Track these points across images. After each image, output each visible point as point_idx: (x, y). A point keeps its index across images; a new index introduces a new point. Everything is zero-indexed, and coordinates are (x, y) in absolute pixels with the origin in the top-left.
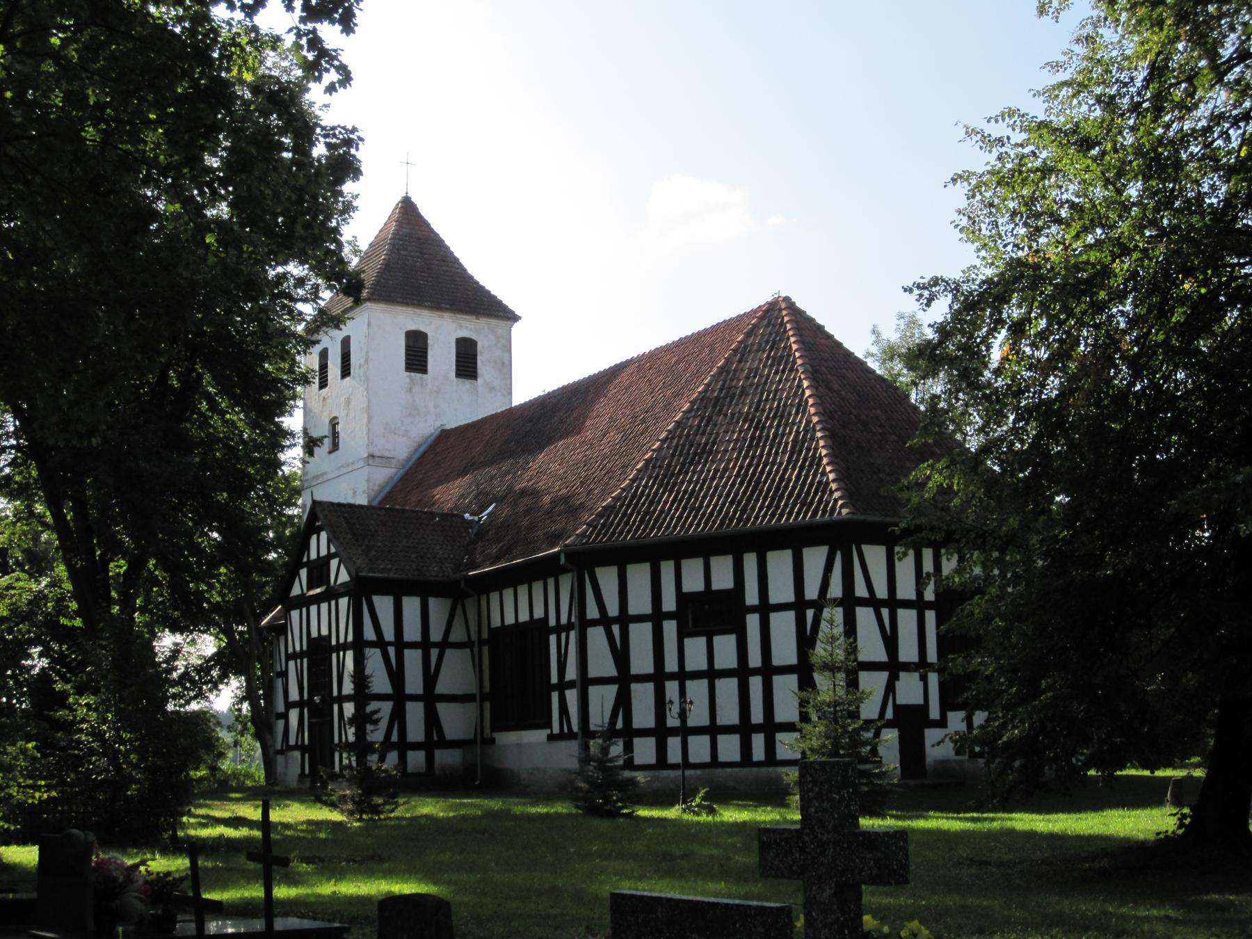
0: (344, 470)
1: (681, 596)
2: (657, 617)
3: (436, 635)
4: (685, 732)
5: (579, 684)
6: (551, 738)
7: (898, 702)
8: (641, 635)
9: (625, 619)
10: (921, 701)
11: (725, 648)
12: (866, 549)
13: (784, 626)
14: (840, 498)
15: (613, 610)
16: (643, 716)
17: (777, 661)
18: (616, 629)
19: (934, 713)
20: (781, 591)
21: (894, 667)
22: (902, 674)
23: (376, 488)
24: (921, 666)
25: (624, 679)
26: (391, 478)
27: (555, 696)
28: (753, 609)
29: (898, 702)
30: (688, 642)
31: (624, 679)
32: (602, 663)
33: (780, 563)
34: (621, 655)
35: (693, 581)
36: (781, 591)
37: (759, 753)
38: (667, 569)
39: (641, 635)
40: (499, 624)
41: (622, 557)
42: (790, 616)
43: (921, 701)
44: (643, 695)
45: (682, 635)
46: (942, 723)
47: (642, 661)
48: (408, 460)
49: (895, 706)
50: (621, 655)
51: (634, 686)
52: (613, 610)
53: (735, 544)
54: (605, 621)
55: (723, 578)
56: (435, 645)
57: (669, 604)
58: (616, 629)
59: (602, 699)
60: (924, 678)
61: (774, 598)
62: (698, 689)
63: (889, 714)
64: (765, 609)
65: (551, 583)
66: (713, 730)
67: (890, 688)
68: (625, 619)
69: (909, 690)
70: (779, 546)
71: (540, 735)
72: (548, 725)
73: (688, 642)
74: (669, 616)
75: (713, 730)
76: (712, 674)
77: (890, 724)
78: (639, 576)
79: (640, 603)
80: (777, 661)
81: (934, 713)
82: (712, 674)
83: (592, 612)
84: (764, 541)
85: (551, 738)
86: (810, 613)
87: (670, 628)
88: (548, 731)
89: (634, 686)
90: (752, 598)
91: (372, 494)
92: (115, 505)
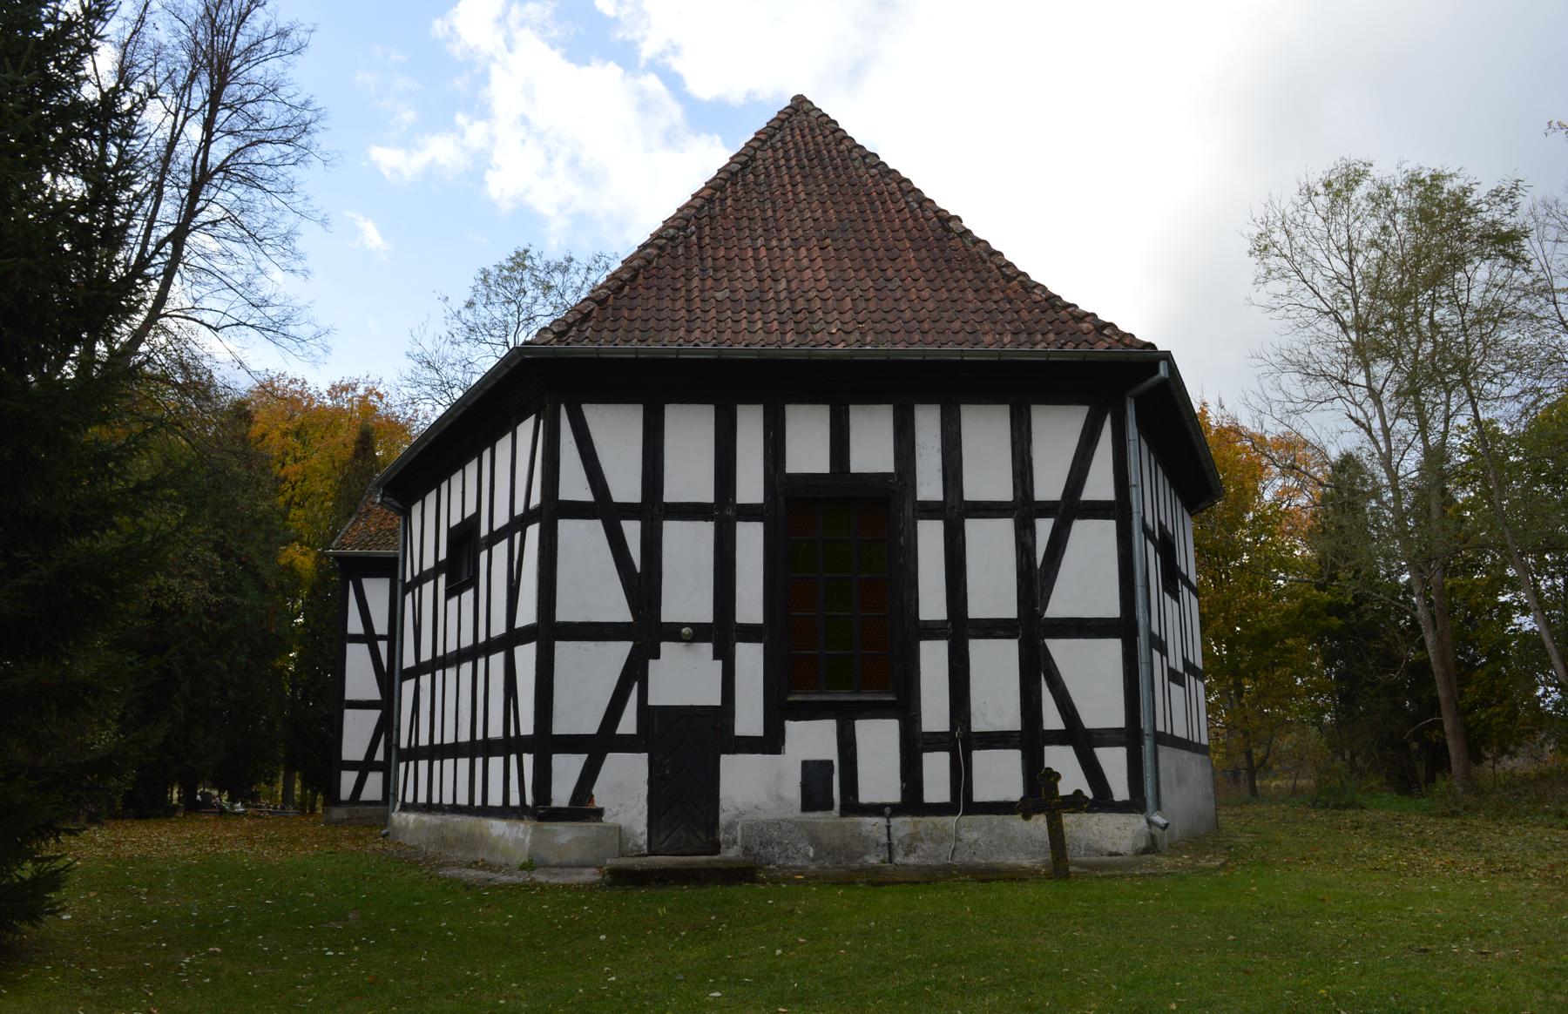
3: (1049, 485)
7: (652, 701)
9: (655, 509)
10: (716, 700)
12: (594, 415)
13: (992, 549)
15: (626, 486)
17: (977, 609)
18: (632, 530)
19: (749, 719)
20: (987, 478)
21: (646, 632)
22: (666, 647)
24: (722, 633)
25: (1032, 629)
28: (749, 513)
29: (652, 701)
33: (986, 433)
34: (643, 584)
35: (808, 451)
36: (987, 478)
37: (936, 786)
38: (750, 425)
42: (1004, 528)
43: (716, 700)
46: (771, 742)
49: (643, 708)
50: (643, 584)
52: (626, 486)
53: (902, 383)
54: (604, 509)
55: (872, 450)
56: (1046, 509)
57: (750, 488)
58: (632, 530)
60: (725, 655)
61: (674, 492)
63: (628, 724)
64: (956, 512)
67: (634, 674)
68: (655, 509)
69: (683, 678)
70: (689, 395)
74: (929, 510)
77: (627, 744)
78: (689, 434)
79: (689, 478)
80: (977, 609)
81: (749, 719)
83: (574, 486)
84: (953, 383)
86: (1044, 527)
90: (929, 487)
92: (55, 134)
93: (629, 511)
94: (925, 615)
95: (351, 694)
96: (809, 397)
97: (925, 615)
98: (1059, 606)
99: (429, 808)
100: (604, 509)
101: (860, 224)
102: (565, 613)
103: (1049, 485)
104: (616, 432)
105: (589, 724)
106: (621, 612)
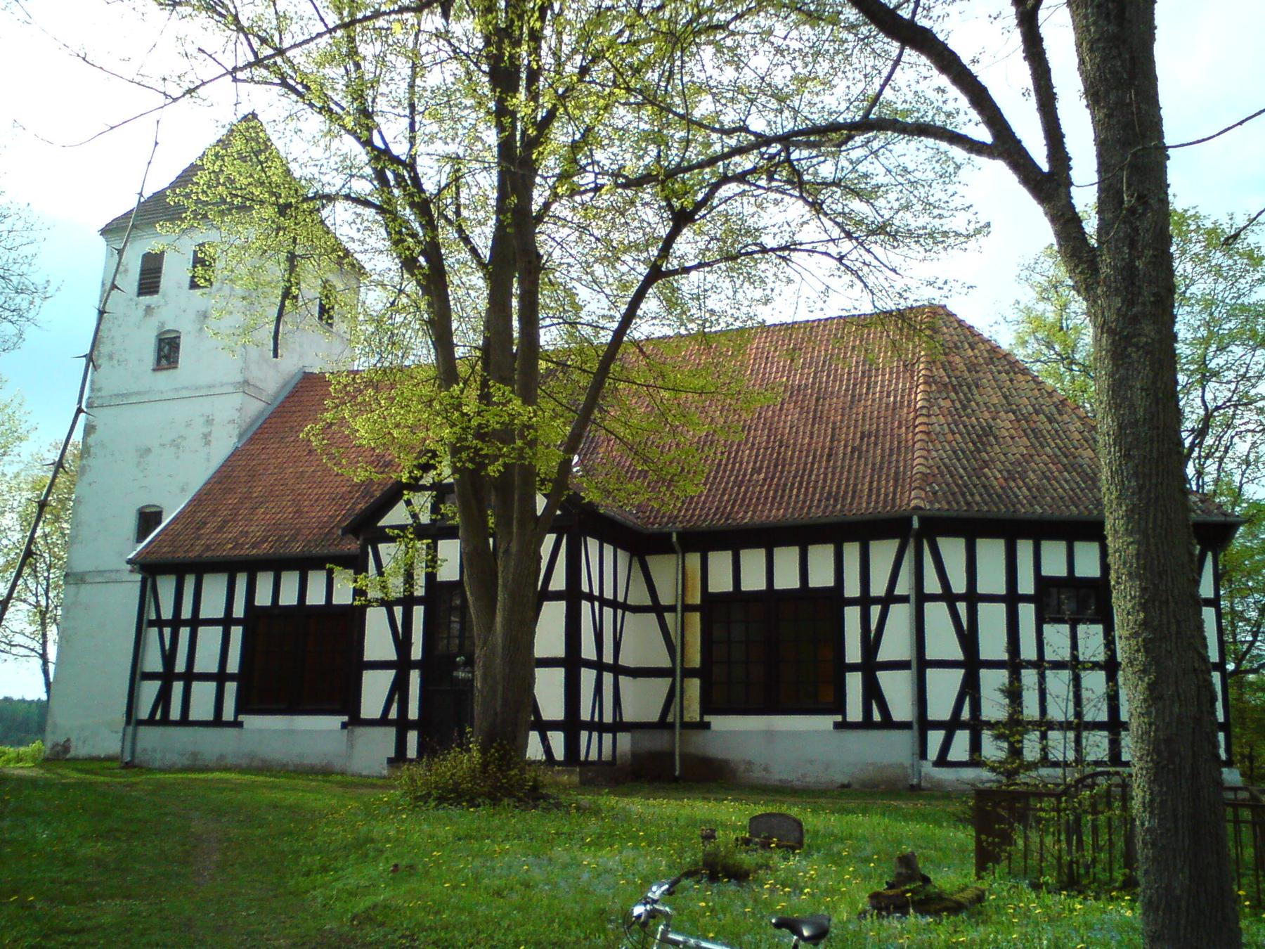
0: (185, 393)
1: (1039, 579)
2: (1012, 599)
3: (878, 588)
4: (1045, 725)
5: (914, 665)
6: (843, 726)
8: (992, 619)
9: (973, 598)
11: (1092, 639)
14: (999, 509)
15: (959, 585)
16: (994, 707)
18: (962, 607)
23: (248, 420)
26: (262, 412)
27: (233, 666)
30: (1048, 629)
31: (972, 664)
32: (943, 641)
34: (969, 639)
35: (1054, 564)
38: (1025, 549)
39: (992, 619)
40: (795, 584)
41: (972, 529)
44: (992, 681)
45: (1040, 621)
47: (992, 644)
48: (276, 397)
50: (969, 639)
51: (983, 673)
52: (959, 585)
53: (836, 532)
54: (948, 597)
56: (877, 600)
57: (1026, 585)
59: (944, 689)
62: (1059, 682)
65: (190, 582)
66: (1079, 726)
68: (973, 598)
71: (825, 722)
72: (840, 708)
73: (1048, 629)
74: (852, 602)
75: (1079, 726)
76: (1075, 665)
78: (991, 553)
79: (992, 579)
82: (1075, 665)
84: (866, 530)
85: (837, 726)
87: (1027, 612)
88: (839, 718)
89: (983, 673)
90: (852, 589)
91: (244, 426)
93: (960, 597)
94: (240, 628)
95: (369, 655)
96: (1025, 536)
97: (240, 628)
98: (882, 656)
99: (618, 726)
100: (948, 597)
101: (950, 437)
102: (930, 655)
103: (878, 588)
104: (953, 550)
105: (946, 716)
106: (959, 655)
